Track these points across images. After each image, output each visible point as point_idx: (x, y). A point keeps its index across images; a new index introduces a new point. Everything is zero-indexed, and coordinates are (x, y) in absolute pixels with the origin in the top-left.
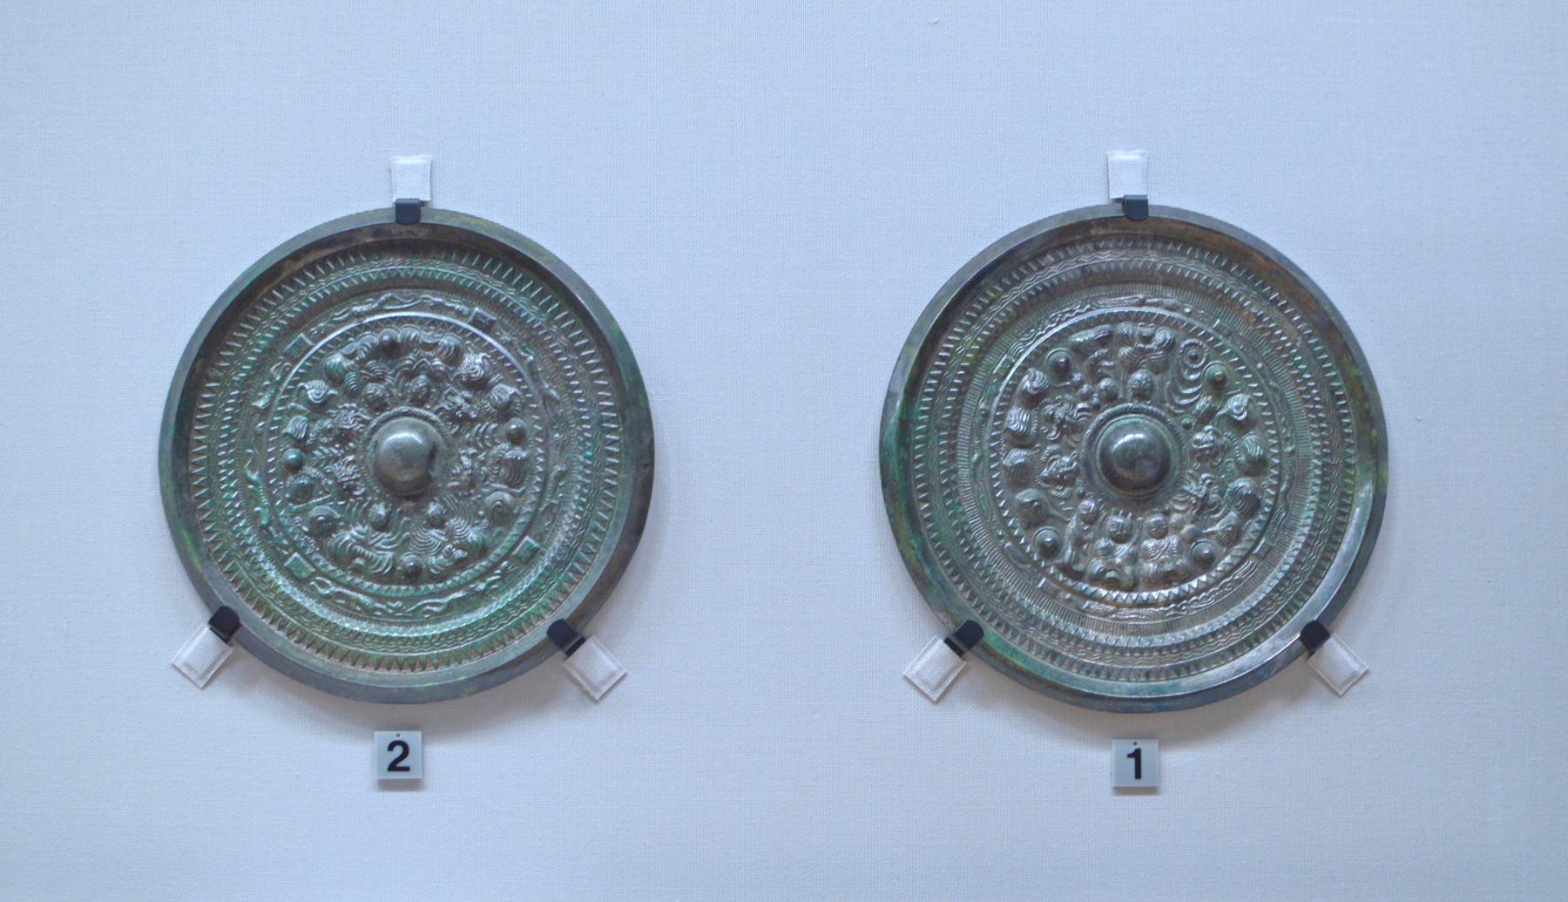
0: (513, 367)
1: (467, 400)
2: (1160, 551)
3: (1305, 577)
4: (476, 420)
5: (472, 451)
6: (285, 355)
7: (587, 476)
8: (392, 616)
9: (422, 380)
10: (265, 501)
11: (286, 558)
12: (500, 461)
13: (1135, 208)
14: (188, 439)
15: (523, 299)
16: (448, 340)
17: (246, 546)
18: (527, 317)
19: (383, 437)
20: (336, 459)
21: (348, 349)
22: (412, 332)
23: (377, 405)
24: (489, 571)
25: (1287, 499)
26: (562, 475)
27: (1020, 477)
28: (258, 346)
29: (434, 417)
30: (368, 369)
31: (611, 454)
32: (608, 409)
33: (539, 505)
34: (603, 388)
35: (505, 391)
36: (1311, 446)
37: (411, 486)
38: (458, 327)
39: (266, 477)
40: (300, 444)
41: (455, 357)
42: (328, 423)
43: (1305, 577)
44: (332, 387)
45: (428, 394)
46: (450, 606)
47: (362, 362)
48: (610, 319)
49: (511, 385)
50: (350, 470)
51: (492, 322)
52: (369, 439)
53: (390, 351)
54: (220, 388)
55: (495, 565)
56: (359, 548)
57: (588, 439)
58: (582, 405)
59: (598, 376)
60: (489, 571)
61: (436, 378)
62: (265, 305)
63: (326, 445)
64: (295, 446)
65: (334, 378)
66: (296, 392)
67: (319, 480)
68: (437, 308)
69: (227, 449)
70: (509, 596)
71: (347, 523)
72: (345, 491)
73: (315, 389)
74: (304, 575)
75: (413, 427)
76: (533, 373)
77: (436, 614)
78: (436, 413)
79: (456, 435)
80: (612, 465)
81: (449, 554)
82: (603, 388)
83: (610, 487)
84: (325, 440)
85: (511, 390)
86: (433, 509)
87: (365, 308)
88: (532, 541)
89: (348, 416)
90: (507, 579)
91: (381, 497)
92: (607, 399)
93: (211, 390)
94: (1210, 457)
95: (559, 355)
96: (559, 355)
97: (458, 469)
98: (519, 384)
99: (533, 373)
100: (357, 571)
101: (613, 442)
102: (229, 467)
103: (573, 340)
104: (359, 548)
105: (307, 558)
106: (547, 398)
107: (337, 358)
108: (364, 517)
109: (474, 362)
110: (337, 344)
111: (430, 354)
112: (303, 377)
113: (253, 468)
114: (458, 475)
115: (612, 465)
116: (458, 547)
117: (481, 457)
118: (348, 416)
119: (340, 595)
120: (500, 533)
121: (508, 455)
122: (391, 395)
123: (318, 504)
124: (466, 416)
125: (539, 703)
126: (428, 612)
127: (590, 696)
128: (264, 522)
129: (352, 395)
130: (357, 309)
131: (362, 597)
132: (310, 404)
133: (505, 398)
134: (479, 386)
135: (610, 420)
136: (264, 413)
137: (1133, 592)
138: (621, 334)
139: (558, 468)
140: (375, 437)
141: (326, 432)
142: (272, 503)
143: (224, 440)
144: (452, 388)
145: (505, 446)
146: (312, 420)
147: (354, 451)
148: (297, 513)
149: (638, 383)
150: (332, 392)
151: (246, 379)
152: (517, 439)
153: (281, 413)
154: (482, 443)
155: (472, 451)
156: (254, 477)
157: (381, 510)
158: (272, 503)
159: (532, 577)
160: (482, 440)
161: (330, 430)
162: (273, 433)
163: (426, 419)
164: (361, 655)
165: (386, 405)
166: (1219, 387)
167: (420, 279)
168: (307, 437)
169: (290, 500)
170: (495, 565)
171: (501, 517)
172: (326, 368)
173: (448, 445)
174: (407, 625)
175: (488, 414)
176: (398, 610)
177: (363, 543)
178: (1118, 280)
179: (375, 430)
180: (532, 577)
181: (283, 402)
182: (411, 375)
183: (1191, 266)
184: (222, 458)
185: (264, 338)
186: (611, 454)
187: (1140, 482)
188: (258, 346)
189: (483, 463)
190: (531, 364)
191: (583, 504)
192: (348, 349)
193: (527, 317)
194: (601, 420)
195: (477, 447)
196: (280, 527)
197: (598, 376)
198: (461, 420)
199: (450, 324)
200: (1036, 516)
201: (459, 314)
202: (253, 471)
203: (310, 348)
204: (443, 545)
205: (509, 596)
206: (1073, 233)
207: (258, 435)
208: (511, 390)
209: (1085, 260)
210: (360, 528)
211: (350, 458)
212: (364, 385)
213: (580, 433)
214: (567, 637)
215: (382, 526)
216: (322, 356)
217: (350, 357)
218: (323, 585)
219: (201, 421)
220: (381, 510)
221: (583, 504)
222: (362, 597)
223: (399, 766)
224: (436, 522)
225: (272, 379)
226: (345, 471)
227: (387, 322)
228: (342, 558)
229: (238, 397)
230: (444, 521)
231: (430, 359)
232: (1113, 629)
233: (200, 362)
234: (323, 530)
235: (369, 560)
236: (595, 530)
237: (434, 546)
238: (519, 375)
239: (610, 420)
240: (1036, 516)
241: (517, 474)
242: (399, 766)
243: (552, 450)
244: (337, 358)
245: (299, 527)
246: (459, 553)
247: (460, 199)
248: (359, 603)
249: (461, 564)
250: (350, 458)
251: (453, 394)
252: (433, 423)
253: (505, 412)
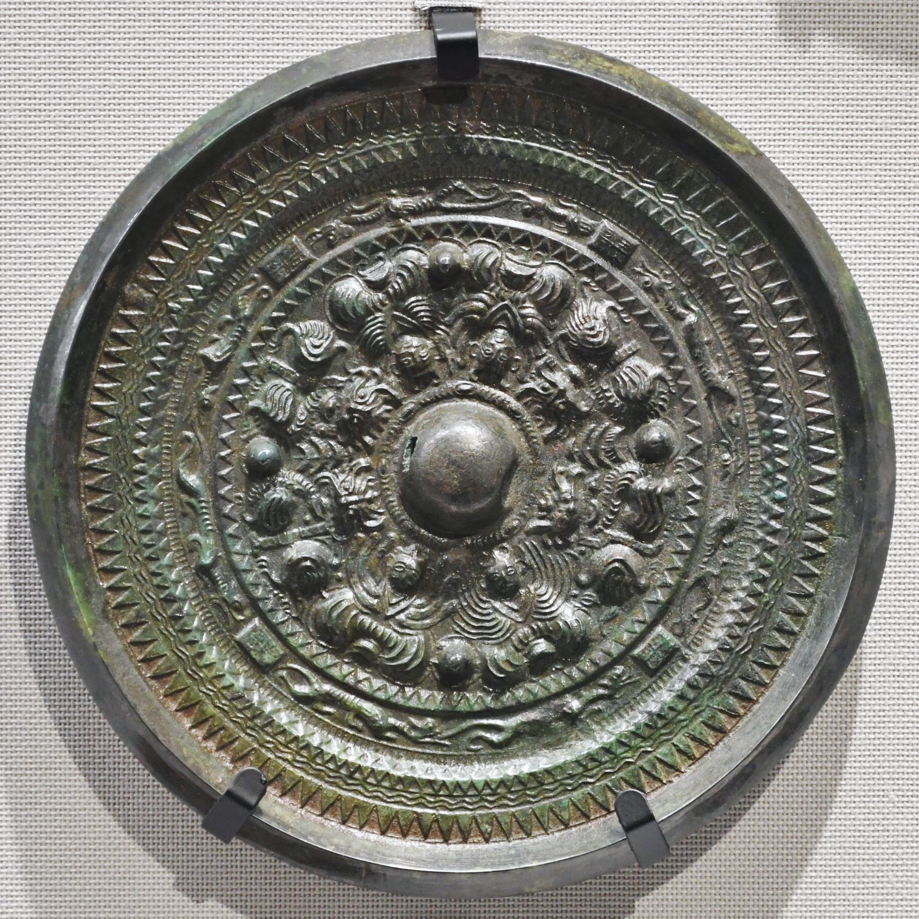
0: (661, 330)
1: (574, 379)
4: (587, 416)
5: (576, 468)
6: (262, 271)
7: (774, 533)
8: (415, 742)
9: (498, 339)
10: (209, 519)
11: (239, 625)
12: (626, 493)
14: (82, 404)
15: (688, 214)
16: (552, 272)
17: (170, 600)
18: (693, 246)
19: (436, 421)
20: (338, 463)
21: (374, 273)
22: (482, 251)
23: (416, 376)
24: (589, 680)
26: (728, 527)
28: (218, 252)
29: (514, 404)
30: (407, 311)
31: (822, 500)
32: (821, 420)
33: (685, 575)
34: (816, 382)
35: (642, 369)
37: (455, 520)
38: (572, 252)
39: (215, 481)
40: (276, 429)
41: (558, 304)
42: (329, 398)
44: (341, 335)
45: (507, 365)
46: (517, 734)
47: (398, 298)
48: (838, 264)
49: (654, 362)
50: (360, 483)
51: (632, 249)
52: (399, 432)
53: (445, 281)
54: (146, 320)
55: (601, 671)
56: (368, 620)
57: (783, 470)
58: (778, 409)
59: (808, 362)
60: (589, 680)
61: (527, 339)
62: (237, 182)
63: (323, 435)
64: (269, 433)
65: (347, 320)
66: (276, 335)
67: (303, 494)
68: (533, 214)
69: (149, 427)
70: (623, 725)
71: (349, 574)
72: (347, 522)
73: (316, 336)
74: (268, 658)
75: (481, 419)
76: (692, 344)
77: (491, 744)
78: (518, 398)
79: (548, 440)
80: (820, 519)
81: (524, 645)
82: (816, 382)
83: (815, 557)
84: (321, 426)
85: (654, 370)
86: (502, 559)
87: (412, 202)
88: (668, 636)
89: (365, 389)
90: (617, 698)
91: (411, 536)
92: (821, 402)
93: (127, 321)
95: (744, 319)
96: (744, 319)
97: (549, 498)
98: (669, 362)
99: (692, 344)
100: (363, 659)
101: (826, 480)
102: (149, 458)
103: (770, 296)
104: (368, 620)
105: (273, 628)
106: (716, 393)
107: (351, 288)
108: (380, 566)
109: (592, 314)
110: (355, 261)
111: (521, 295)
112: (291, 312)
113: (192, 460)
114: (548, 509)
115: (820, 519)
116: (539, 634)
117: (592, 481)
118: (365, 389)
119: (329, 699)
120: (614, 617)
121: (641, 484)
122: (444, 360)
123: (303, 537)
124: (571, 407)
126: (480, 739)
128: (207, 560)
129: (374, 353)
130: (397, 202)
131: (368, 707)
132: (300, 362)
133: (644, 384)
134: (597, 358)
135: (823, 440)
136: (216, 370)
138: (855, 291)
139: (722, 515)
140: (409, 430)
141: (326, 414)
142: (221, 529)
143: (144, 412)
144: (550, 356)
145: (633, 466)
146: (304, 389)
147: (369, 450)
148: (263, 549)
150: (340, 343)
151: (192, 307)
152: (654, 456)
153: (246, 372)
154: (597, 459)
155: (576, 468)
156: (193, 480)
157: (408, 558)
158: (221, 529)
159: (662, 697)
160: (595, 454)
161: (331, 411)
162: (232, 406)
163: (501, 406)
164: (358, 806)
165: (434, 375)
167: (513, 161)
168: (289, 421)
169: (253, 525)
170: (601, 671)
171: (615, 589)
172: (333, 295)
173: (535, 453)
174: (438, 759)
175: (610, 410)
176: (428, 732)
177: (374, 612)
179: (409, 417)
180: (662, 697)
181: (253, 354)
182: (479, 327)
184: (139, 443)
185: (230, 239)
186: (822, 500)
188: (218, 252)
189: (594, 492)
190: (690, 329)
191: (763, 581)
192: (374, 273)
193: (693, 246)
194: (808, 440)
195: (586, 464)
196: (235, 571)
197: (808, 362)
198: (557, 412)
199: (556, 244)
201: (574, 230)
202: (192, 470)
203: (310, 261)
204: (512, 630)
205: (623, 725)
207: (205, 408)
208: (654, 370)
209: (463, 510)
210: (370, 583)
211: (363, 461)
212: (396, 338)
213: (768, 457)
215: (405, 586)
216: (326, 278)
217: (374, 286)
218: (303, 679)
219: (107, 376)
220: (408, 558)
221: (763, 581)
222: (368, 707)
224: (503, 589)
225: (235, 311)
226: (351, 484)
227: (445, 231)
228: (340, 637)
229: (178, 337)
230: (517, 587)
231: (516, 302)
233: (113, 274)
234: (305, 583)
235: (384, 643)
236: (780, 630)
237: (488, 636)
238: (669, 345)
239: (823, 440)
241: (648, 517)
243: (715, 481)
244: (351, 288)
245: (260, 575)
246: (542, 646)
248: (359, 715)
249: (540, 665)
250: (363, 461)
251: (551, 367)
252: (513, 414)
253: (636, 410)
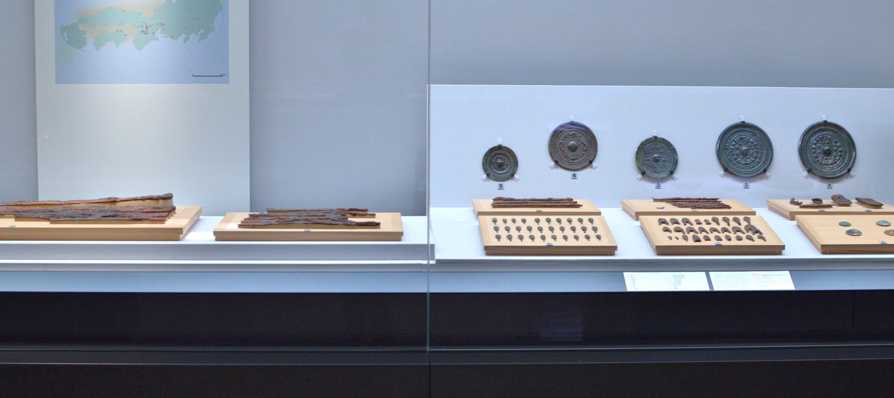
2: (830, 161)
3: (847, 164)
13: (825, 122)
25: (845, 155)
27: (814, 153)
36: (847, 149)
43: (847, 164)
94: (836, 150)
109: (752, 140)
118: (737, 146)
125: (762, 179)
127: (767, 178)
137: (830, 165)
149: (647, 140)
166: (836, 142)
178: (824, 130)
183: (832, 129)
187: (827, 153)
200: (816, 157)
206: (819, 125)
214: (765, 171)
223: (746, 187)
232: (827, 170)
240: (816, 157)
241: (757, 152)
242: (746, 187)
247: (749, 120)
